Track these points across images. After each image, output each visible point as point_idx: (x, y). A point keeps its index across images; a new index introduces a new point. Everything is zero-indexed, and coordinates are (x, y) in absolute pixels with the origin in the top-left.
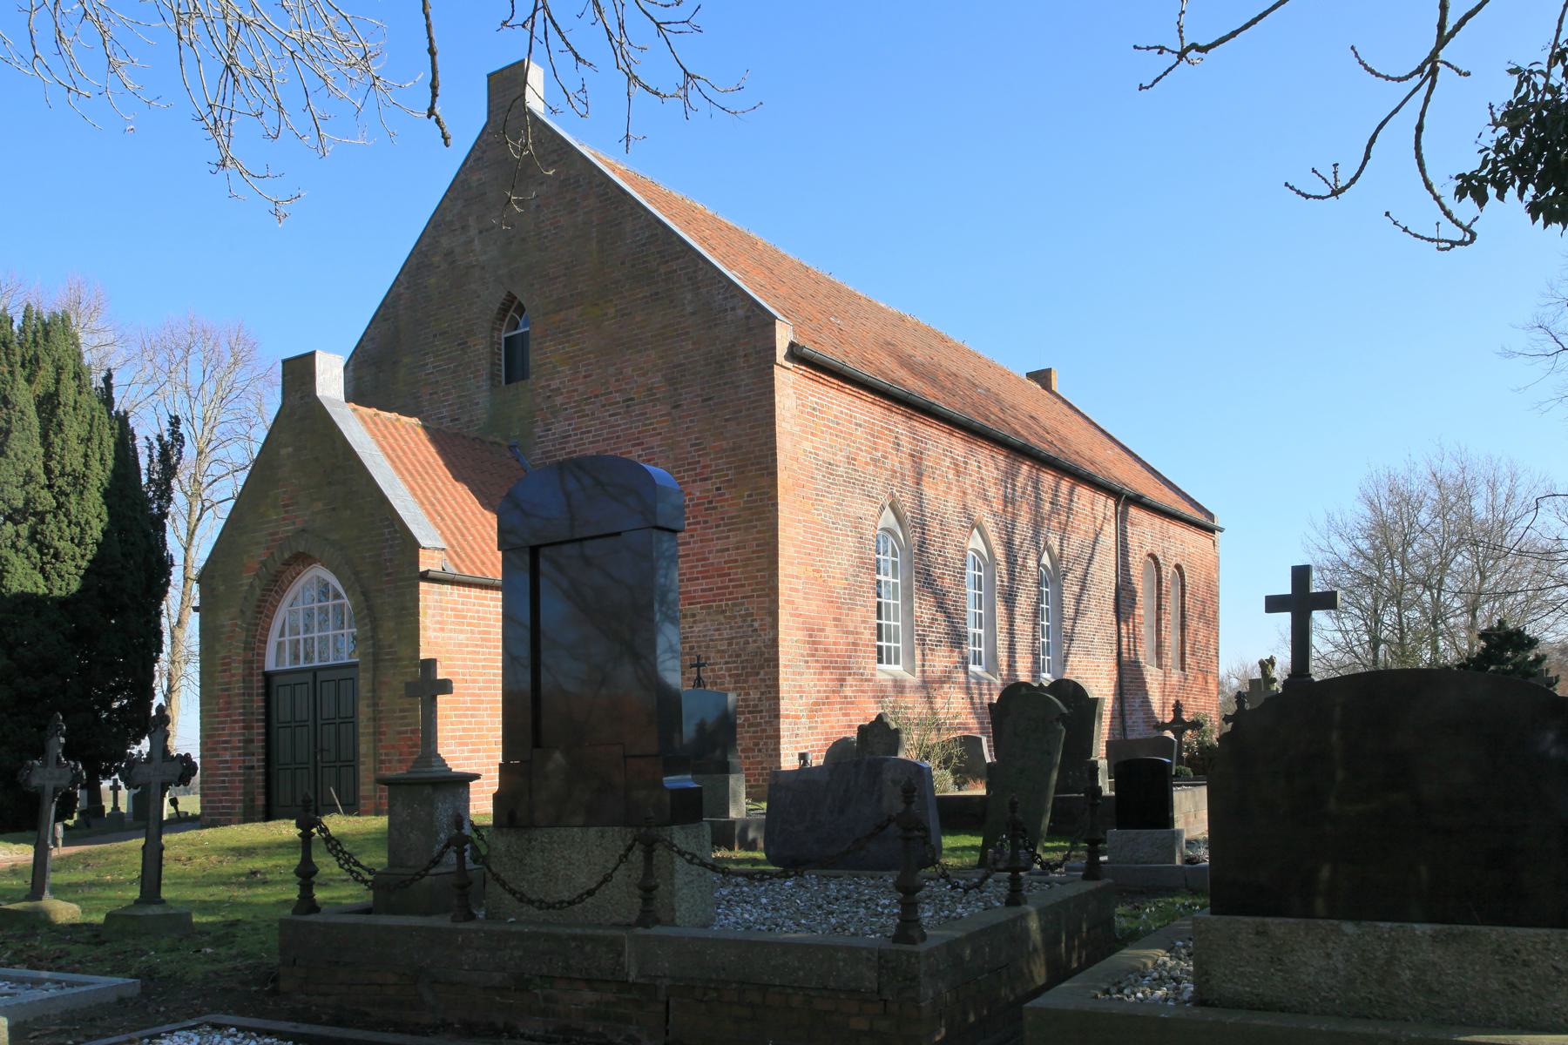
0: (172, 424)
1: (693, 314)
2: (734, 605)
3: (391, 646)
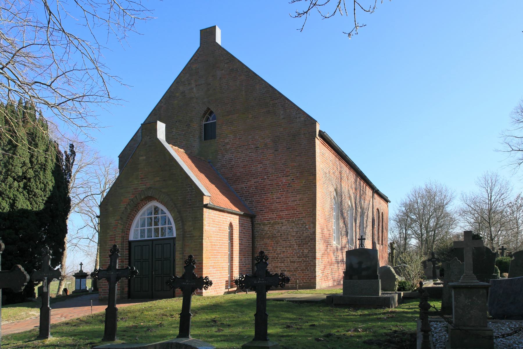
0: (70, 147)
1: (283, 118)
3: (190, 232)
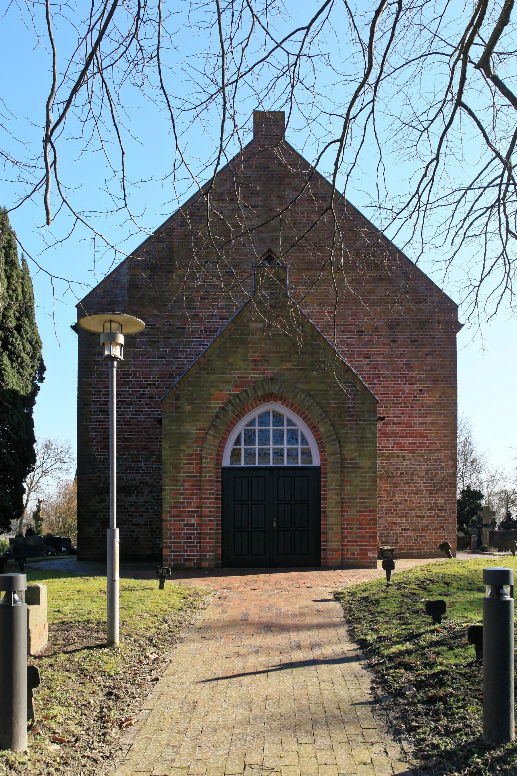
2: (429, 453)
3: (351, 459)
